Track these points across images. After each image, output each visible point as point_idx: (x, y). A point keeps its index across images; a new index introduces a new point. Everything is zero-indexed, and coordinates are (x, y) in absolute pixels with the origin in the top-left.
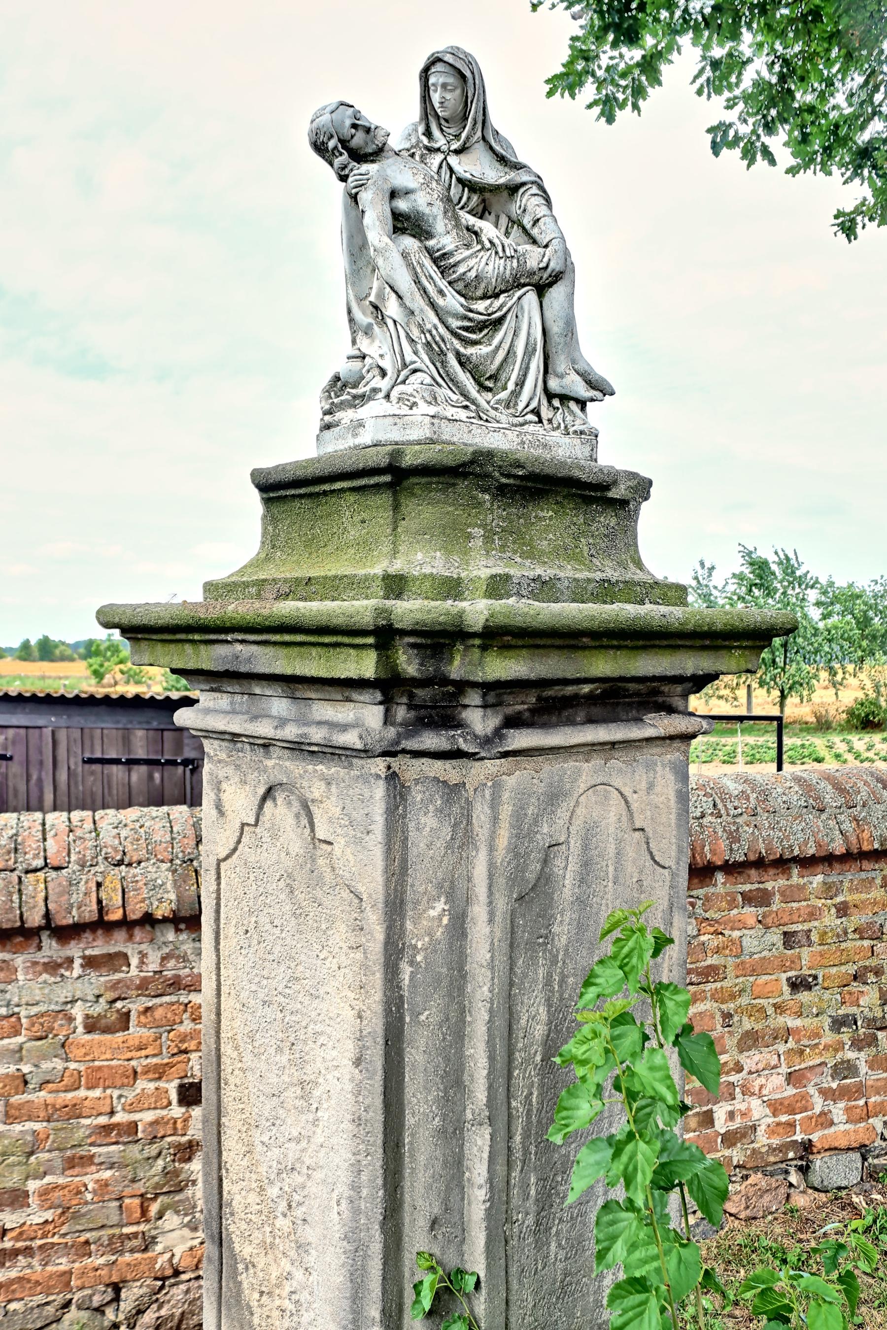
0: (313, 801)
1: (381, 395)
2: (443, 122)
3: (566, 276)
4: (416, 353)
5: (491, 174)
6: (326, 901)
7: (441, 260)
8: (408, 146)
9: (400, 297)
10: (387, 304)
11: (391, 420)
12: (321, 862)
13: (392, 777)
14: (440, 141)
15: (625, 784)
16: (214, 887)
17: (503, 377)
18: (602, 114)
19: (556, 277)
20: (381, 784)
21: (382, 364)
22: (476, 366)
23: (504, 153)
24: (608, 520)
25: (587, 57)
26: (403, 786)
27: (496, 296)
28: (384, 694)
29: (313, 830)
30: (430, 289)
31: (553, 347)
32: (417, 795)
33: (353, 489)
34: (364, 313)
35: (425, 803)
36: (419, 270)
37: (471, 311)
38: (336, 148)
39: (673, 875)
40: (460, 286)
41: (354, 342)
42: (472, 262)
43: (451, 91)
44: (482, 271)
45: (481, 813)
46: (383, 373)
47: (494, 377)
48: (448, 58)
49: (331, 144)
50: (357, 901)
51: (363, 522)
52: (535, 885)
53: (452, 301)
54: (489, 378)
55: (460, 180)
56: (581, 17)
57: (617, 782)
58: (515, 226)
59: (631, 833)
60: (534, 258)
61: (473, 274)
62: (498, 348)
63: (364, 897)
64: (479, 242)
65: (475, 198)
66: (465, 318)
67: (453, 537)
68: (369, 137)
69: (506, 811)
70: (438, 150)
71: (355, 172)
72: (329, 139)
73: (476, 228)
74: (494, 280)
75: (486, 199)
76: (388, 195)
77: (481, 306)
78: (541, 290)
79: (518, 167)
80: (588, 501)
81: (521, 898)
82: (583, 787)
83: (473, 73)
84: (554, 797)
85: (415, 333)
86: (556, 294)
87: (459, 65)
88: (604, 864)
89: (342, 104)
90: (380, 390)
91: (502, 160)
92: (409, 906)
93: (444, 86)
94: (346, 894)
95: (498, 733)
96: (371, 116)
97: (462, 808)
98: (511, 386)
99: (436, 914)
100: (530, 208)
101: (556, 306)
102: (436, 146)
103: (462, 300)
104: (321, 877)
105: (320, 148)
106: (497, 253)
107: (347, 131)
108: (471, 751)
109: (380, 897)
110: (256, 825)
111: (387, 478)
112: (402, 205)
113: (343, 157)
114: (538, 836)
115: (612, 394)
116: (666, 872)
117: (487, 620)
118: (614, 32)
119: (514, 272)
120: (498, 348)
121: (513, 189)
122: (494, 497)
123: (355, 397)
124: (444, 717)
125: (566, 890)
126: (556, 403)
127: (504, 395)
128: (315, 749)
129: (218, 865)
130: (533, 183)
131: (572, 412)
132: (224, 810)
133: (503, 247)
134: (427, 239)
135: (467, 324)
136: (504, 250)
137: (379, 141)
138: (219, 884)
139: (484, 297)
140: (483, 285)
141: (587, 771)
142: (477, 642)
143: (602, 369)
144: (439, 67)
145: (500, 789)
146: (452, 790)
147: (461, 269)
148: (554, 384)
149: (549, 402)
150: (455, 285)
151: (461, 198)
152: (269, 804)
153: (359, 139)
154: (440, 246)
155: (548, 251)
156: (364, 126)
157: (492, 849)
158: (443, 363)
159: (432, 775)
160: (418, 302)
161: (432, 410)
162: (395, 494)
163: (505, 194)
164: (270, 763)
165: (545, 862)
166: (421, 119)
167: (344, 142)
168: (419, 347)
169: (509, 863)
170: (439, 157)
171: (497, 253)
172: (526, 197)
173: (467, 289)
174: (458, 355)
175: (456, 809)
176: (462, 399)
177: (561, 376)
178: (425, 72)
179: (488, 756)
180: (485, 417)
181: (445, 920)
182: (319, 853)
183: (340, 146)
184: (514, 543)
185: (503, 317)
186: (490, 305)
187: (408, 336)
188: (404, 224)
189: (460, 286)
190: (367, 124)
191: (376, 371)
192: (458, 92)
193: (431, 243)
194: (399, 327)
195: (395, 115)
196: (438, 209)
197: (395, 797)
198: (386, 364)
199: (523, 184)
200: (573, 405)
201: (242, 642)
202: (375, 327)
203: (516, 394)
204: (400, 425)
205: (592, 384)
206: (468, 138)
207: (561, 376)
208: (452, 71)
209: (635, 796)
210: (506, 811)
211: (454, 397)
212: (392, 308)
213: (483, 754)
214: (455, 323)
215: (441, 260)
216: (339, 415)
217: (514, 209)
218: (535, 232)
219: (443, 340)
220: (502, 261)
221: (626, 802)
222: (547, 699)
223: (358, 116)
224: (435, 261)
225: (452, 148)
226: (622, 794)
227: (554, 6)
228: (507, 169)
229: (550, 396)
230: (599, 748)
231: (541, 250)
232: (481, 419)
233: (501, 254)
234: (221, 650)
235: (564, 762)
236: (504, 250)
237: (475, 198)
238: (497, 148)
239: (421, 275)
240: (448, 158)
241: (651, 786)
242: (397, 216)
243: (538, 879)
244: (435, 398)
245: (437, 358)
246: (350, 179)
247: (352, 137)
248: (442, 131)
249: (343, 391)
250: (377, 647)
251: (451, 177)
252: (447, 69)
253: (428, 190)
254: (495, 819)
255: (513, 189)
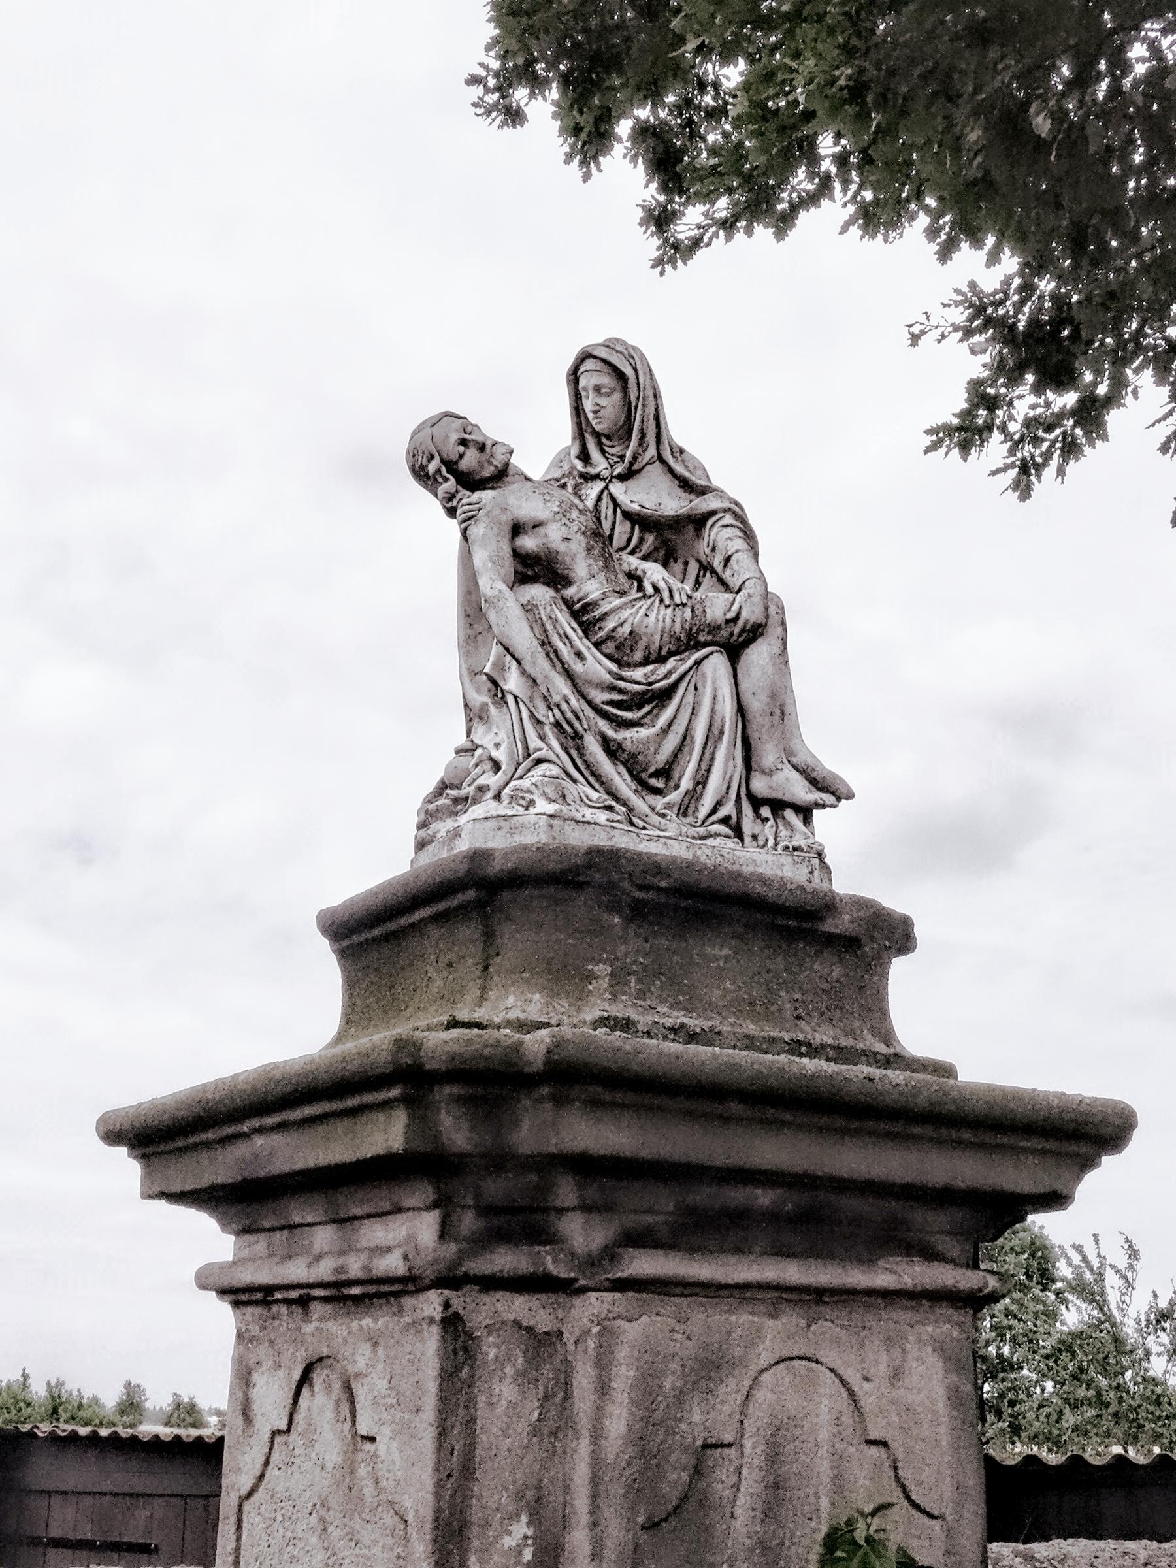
0: (357, 1375)
1: (490, 794)
2: (604, 440)
3: (774, 631)
4: (542, 738)
5: (667, 502)
6: (366, 1536)
7: (584, 616)
8: (557, 474)
9: (519, 662)
10: (507, 675)
11: (492, 824)
12: (362, 1471)
13: (452, 1323)
14: (600, 465)
15: (848, 1364)
16: (233, 1545)
17: (676, 775)
18: (1016, 486)
19: (755, 632)
20: (435, 1329)
21: (495, 754)
22: (633, 756)
23: (687, 474)
24: (827, 968)
25: (992, 404)
26: (471, 1337)
27: (662, 660)
28: (438, 1190)
29: (354, 1423)
30: (565, 652)
31: (754, 729)
32: (490, 1350)
33: (436, 918)
34: (478, 690)
35: (500, 1362)
36: (549, 626)
37: (622, 679)
38: (438, 471)
39: (949, 1533)
40: (610, 647)
41: (469, 733)
42: (625, 614)
43: (608, 395)
44: (639, 625)
45: (584, 1377)
46: (497, 766)
47: (665, 773)
48: (603, 353)
49: (432, 468)
50: (402, 1527)
51: (450, 965)
52: (677, 1507)
53: (596, 666)
54: (657, 774)
55: (627, 515)
56: (984, 351)
57: (830, 1356)
58: (708, 574)
59: (864, 1446)
60: (717, 605)
61: (626, 629)
62: (666, 730)
63: (410, 1518)
64: (640, 588)
65: (650, 539)
66: (612, 688)
67: (565, 976)
68: (484, 457)
69: (623, 1377)
70: (597, 476)
71: (464, 501)
72: (429, 461)
73: (639, 573)
74: (657, 637)
75: (670, 537)
76: (507, 529)
77: (639, 673)
78: (734, 652)
79: (702, 491)
80: (791, 936)
81: (652, 1526)
82: (766, 1358)
83: (635, 369)
84: (710, 1368)
85: (542, 712)
86: (758, 655)
87: (615, 359)
88: (812, 1490)
89: (448, 415)
90: (488, 787)
91: (686, 485)
92: (475, 1531)
93: (597, 389)
94: (389, 1519)
95: (610, 1254)
96: (491, 429)
97: (557, 1371)
98: (686, 783)
99: (514, 1543)
100: (720, 545)
101: (756, 672)
102: (593, 471)
103: (614, 667)
104: (361, 1498)
105: (421, 474)
106: (662, 601)
107: (452, 450)
108: (564, 1275)
109: (428, 1513)
110: (288, 1431)
111: (471, 894)
112: (529, 543)
113: (449, 483)
114: (683, 1426)
115: (850, 796)
116: (936, 1525)
117: (549, 1052)
118: (1036, 373)
119: (687, 626)
120: (666, 730)
121: (699, 522)
122: (629, 921)
123: (456, 801)
124: (526, 1223)
125: (738, 1524)
126: (766, 812)
127: (675, 797)
128: (356, 1291)
129: (240, 1506)
130: (725, 511)
131: (789, 826)
132: (251, 1414)
133: (671, 591)
134: (564, 587)
135: (616, 697)
136: (671, 596)
137: (498, 461)
138: (238, 1539)
139: (646, 661)
140: (642, 645)
141: (775, 1333)
142: (545, 1090)
143: (831, 763)
144: (589, 364)
145: (620, 1344)
146: (541, 1344)
147: (610, 624)
148: (759, 785)
149: (756, 811)
150: (604, 646)
151: (629, 540)
152: (305, 1392)
153: (470, 460)
154: (581, 594)
155: (739, 598)
156: (476, 442)
157: (597, 1435)
158: (580, 750)
159: (511, 1317)
160: (541, 666)
161: (551, 808)
162: (485, 917)
163: (690, 530)
164: (309, 1328)
165: (698, 1471)
166: (574, 439)
167: (450, 465)
168: (548, 730)
169: (629, 1464)
170: (599, 485)
171: (662, 601)
172: (715, 529)
173: (621, 651)
174: (605, 742)
175: (547, 1372)
176: (606, 797)
177: (769, 773)
178: (574, 376)
179: (591, 1284)
180: (641, 824)
181: (528, 1554)
182: (360, 1456)
183: (444, 469)
184: (661, 988)
185: (674, 687)
186: (653, 672)
187: (532, 715)
188: (538, 568)
189: (610, 647)
190: (480, 439)
191: (488, 765)
192: (617, 396)
193: (570, 592)
194: (521, 704)
195: (537, 436)
196: (578, 545)
197: (455, 1353)
198: (500, 755)
199: (713, 513)
200: (789, 814)
201: (260, 1131)
202: (492, 708)
203: (694, 795)
204: (506, 829)
205: (816, 782)
206: (635, 458)
207: (769, 773)
208: (606, 368)
209: (866, 1385)
210: (623, 1377)
211: (594, 795)
212: (513, 682)
213: (583, 1282)
214: (599, 697)
215: (584, 616)
216: (434, 826)
217: (703, 548)
218: (727, 575)
219: (577, 717)
220: (670, 610)
221: (851, 1393)
222: (692, 1211)
223: (469, 429)
224: (576, 615)
225: (615, 473)
226: (842, 1380)
227: (943, 336)
228: (692, 497)
229: (757, 803)
230: (795, 1297)
231: (730, 596)
232: (632, 824)
233: (667, 601)
234: (240, 1150)
235: (731, 1312)
236: (671, 596)
237: (650, 539)
238: (679, 468)
239: (551, 632)
240: (611, 487)
241: (896, 1375)
242: (518, 555)
243: (685, 1498)
244: (564, 796)
245: (571, 743)
246: (459, 512)
247: (461, 456)
248: (603, 452)
249: (450, 797)
250: (407, 1101)
251: (615, 512)
252: (600, 366)
253: (564, 520)
254: (603, 1388)
255: (699, 522)
